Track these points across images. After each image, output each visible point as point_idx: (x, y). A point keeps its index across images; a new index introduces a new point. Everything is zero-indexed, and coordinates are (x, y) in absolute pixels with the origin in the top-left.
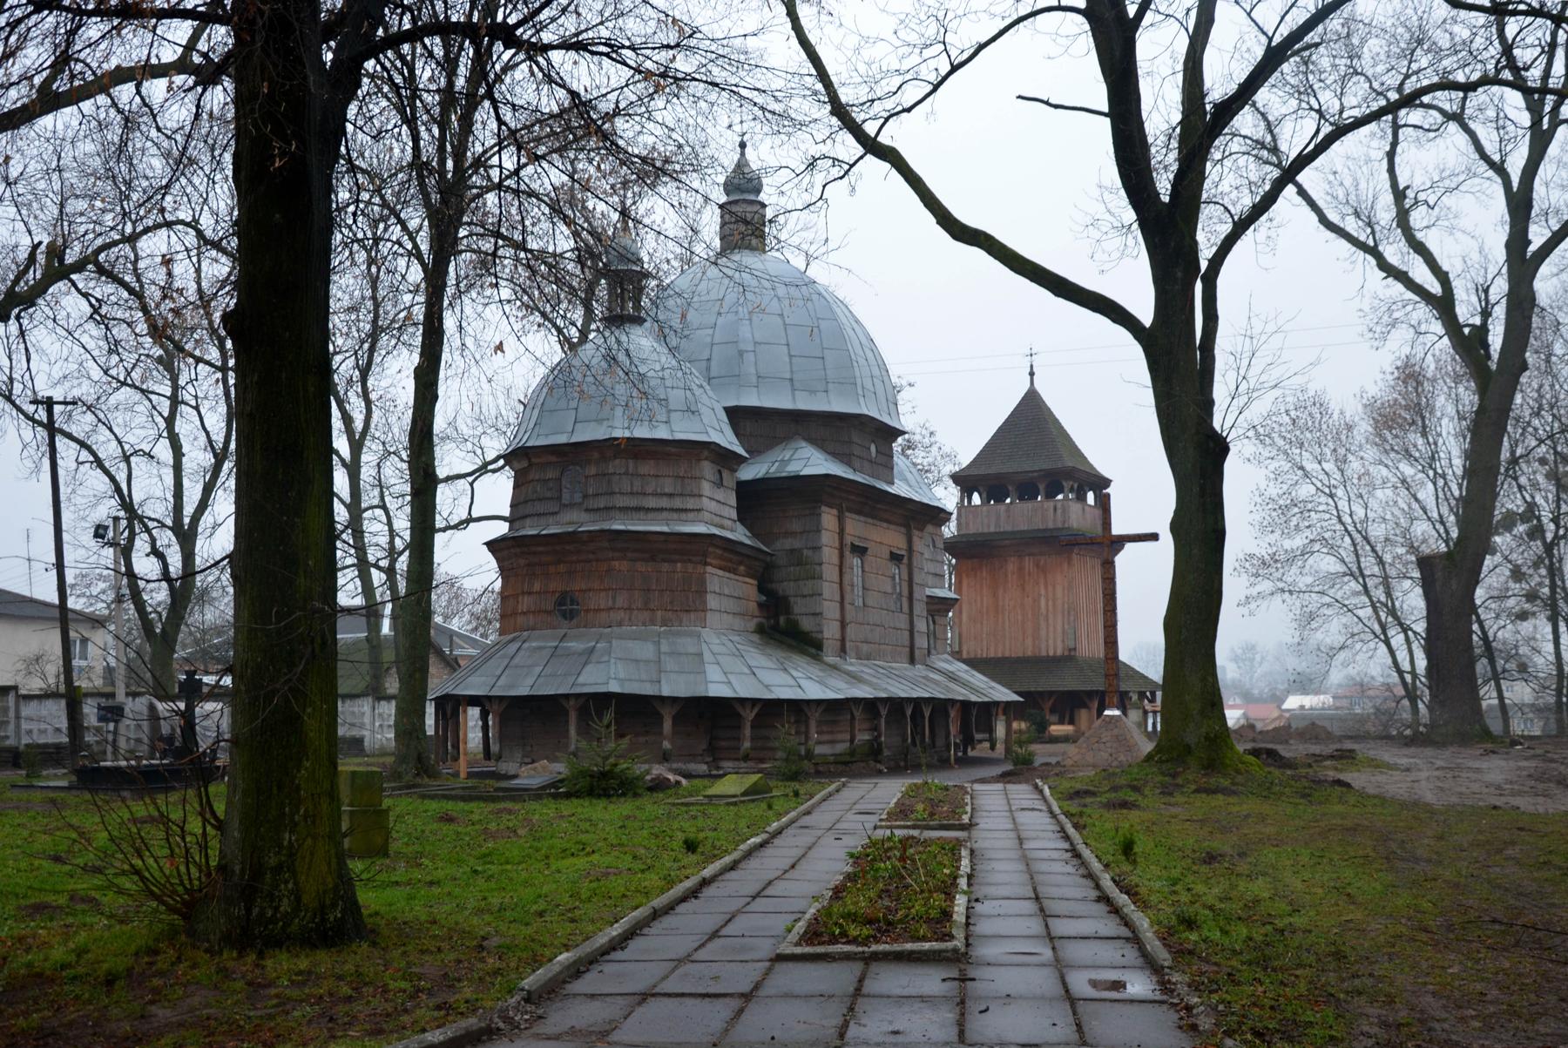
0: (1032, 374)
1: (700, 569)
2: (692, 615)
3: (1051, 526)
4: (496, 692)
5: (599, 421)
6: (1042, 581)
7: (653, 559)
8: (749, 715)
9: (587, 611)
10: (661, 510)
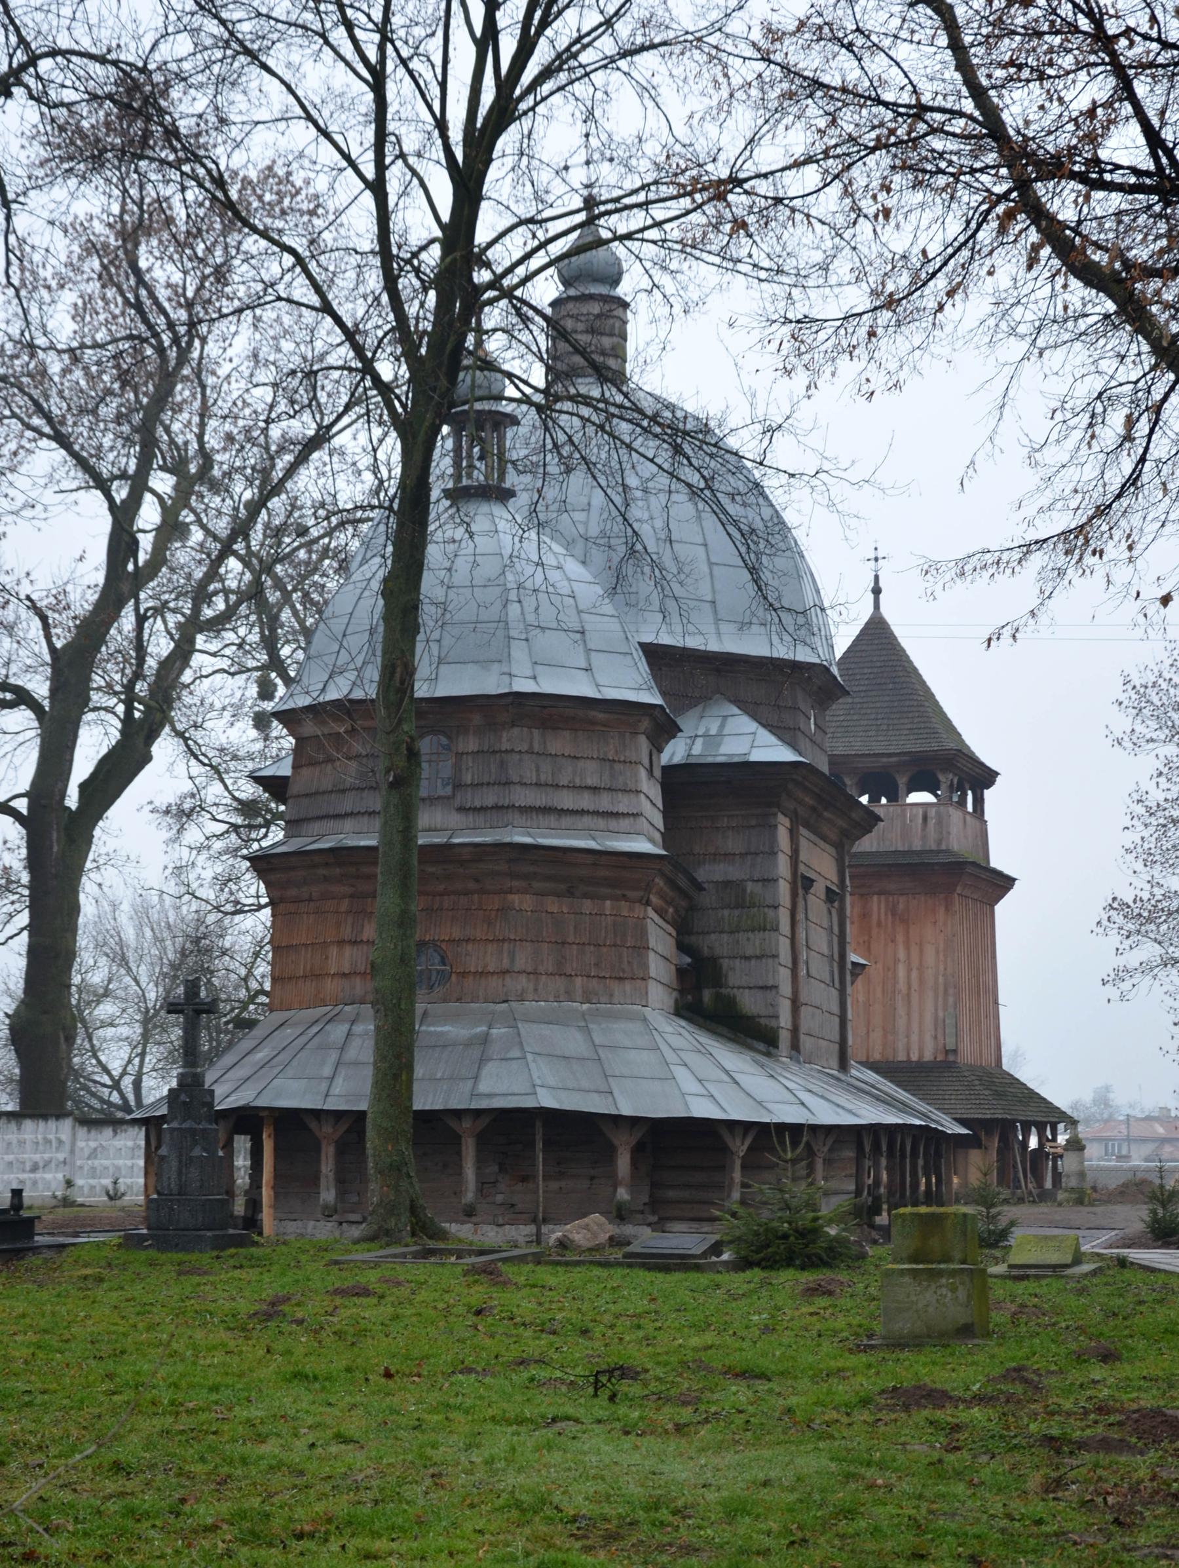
0: (877, 591)
1: (639, 910)
2: (628, 986)
3: (917, 845)
4: (332, 1105)
5: (485, 663)
6: (900, 938)
7: (570, 893)
8: (740, 1147)
9: (464, 974)
10: (582, 812)
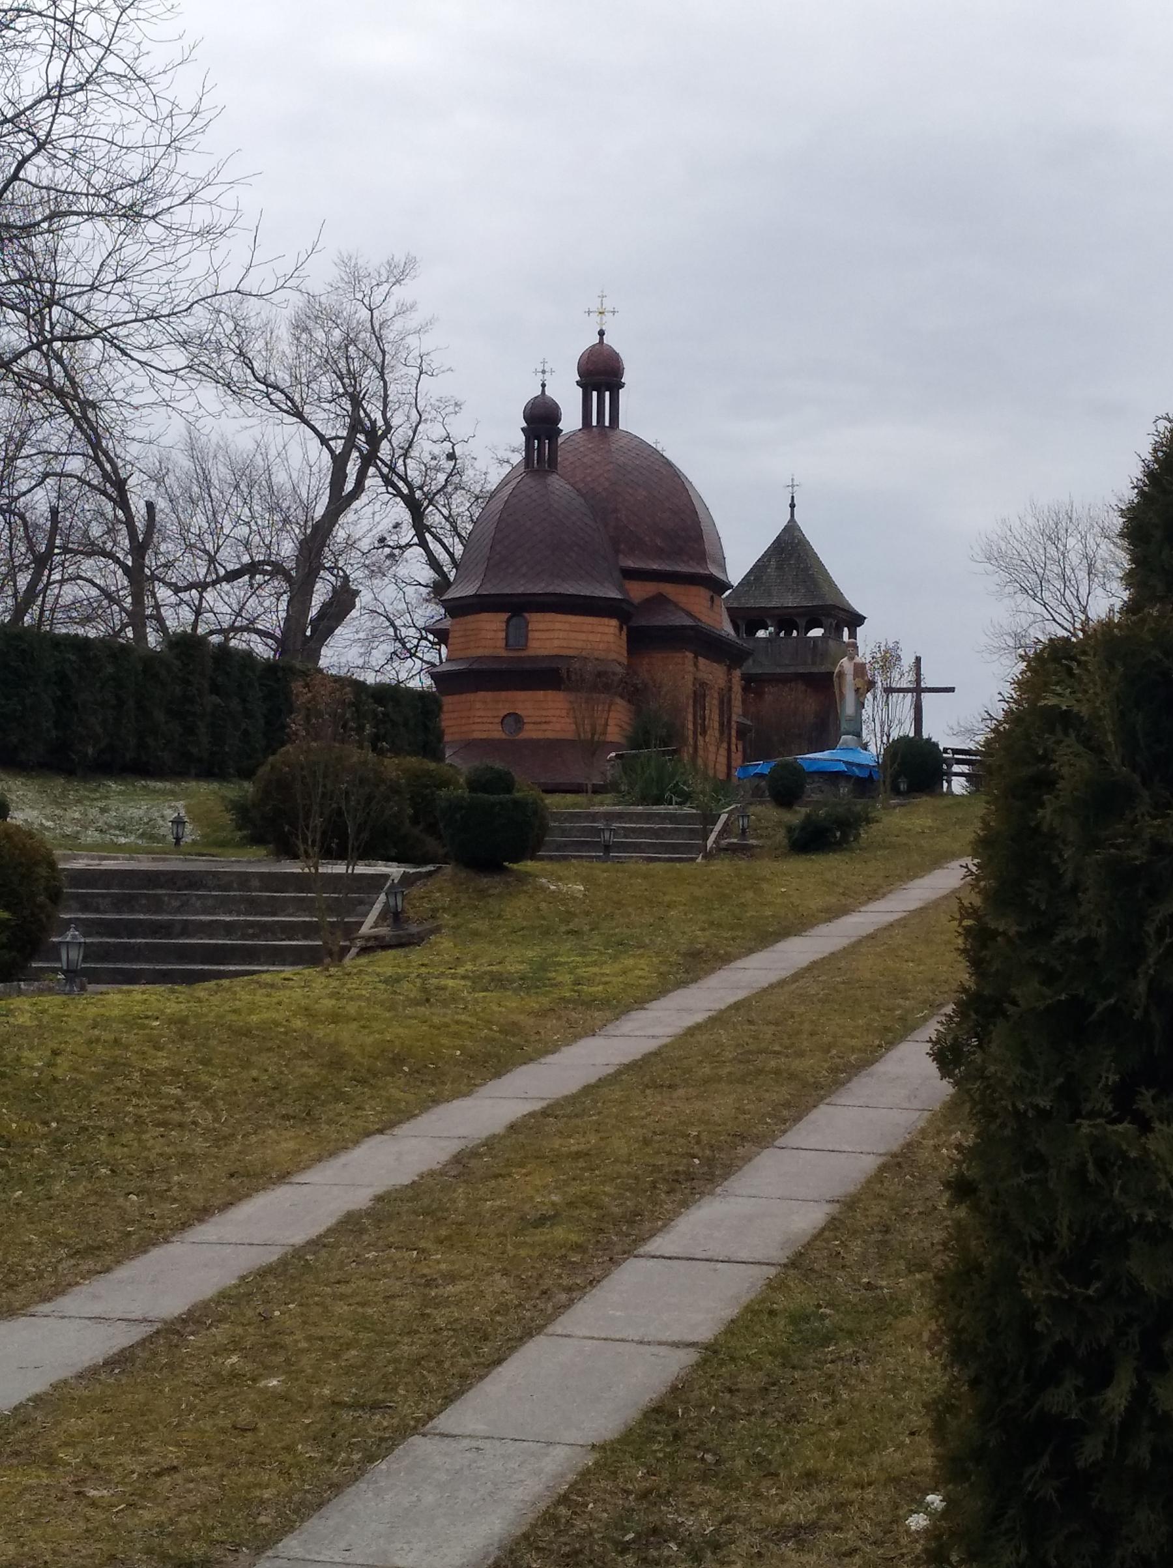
0: (792, 506)
